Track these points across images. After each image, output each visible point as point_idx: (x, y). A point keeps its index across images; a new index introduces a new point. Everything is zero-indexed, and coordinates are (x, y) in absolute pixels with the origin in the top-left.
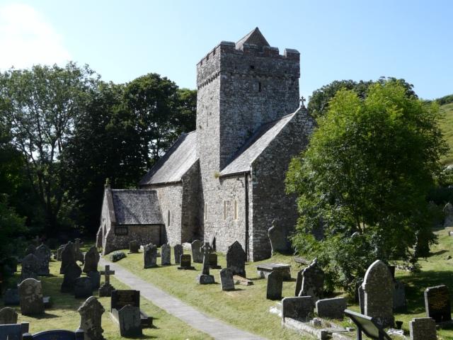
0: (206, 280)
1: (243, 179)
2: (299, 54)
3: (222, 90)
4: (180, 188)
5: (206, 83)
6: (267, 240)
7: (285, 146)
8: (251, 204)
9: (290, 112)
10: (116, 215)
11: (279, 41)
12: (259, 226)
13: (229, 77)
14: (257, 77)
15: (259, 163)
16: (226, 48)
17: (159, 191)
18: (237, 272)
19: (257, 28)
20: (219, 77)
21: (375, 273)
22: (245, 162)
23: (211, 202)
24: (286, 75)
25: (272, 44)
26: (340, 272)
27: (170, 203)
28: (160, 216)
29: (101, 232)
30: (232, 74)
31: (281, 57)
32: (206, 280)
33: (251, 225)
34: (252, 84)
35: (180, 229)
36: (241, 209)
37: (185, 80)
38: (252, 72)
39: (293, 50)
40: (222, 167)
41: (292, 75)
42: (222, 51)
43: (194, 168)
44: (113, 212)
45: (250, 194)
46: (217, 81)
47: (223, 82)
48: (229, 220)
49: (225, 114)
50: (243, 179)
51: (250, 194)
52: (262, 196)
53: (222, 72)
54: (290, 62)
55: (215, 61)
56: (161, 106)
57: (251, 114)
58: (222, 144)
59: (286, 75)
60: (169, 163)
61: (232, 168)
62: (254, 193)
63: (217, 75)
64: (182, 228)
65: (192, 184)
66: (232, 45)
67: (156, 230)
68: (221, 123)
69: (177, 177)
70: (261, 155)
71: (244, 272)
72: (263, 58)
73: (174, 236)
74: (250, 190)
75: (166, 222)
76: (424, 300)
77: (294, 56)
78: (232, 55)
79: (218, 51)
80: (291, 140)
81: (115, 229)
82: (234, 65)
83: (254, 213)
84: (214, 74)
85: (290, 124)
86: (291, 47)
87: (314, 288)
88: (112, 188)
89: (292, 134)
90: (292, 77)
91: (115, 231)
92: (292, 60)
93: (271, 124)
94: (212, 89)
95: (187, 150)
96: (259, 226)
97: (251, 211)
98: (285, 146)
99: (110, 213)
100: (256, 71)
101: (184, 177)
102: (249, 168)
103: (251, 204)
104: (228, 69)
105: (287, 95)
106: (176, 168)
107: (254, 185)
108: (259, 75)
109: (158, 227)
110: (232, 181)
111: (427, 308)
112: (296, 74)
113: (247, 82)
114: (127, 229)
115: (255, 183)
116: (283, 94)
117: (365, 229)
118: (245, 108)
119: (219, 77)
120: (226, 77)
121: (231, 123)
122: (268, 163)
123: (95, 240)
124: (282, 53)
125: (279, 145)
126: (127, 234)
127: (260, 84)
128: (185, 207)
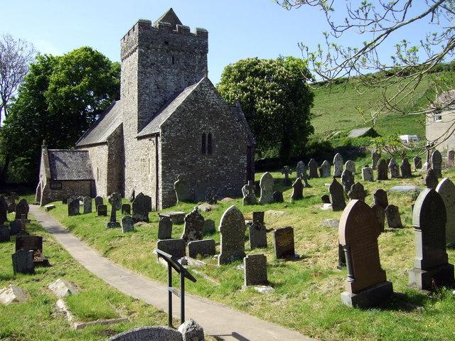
0: (113, 224)
1: (154, 139)
2: (207, 33)
3: (140, 62)
4: (106, 147)
5: (128, 56)
6: (174, 191)
7: (190, 111)
8: (160, 161)
9: (190, 84)
10: (51, 171)
11: (191, 21)
12: (167, 180)
13: (146, 51)
15: (167, 125)
16: (144, 25)
17: (90, 150)
18: (142, 219)
20: (137, 50)
22: (156, 126)
23: (131, 160)
24: (196, 51)
25: (185, 23)
26: (248, 228)
27: (99, 159)
28: (91, 172)
29: (40, 187)
30: (148, 49)
31: (192, 34)
32: (113, 224)
33: (160, 179)
34: (166, 57)
35: (106, 184)
36: (153, 165)
37: (112, 54)
38: (166, 47)
39: (203, 29)
40: (140, 129)
43: (119, 131)
44: (49, 169)
45: (160, 152)
46: (136, 54)
47: (141, 55)
48: (144, 174)
50: (154, 139)
51: (160, 152)
52: (170, 154)
53: (140, 46)
55: (134, 36)
56: (91, 79)
57: (166, 84)
58: (140, 109)
59: (196, 51)
63: (136, 49)
65: (117, 145)
66: (149, 23)
67: (87, 185)
68: (139, 91)
69: (103, 139)
70: (169, 119)
73: (102, 190)
74: (160, 149)
75: (96, 178)
76: (41, 157)
77: (203, 35)
79: (137, 27)
81: (51, 184)
83: (162, 168)
84: (133, 48)
85: (194, 92)
86: (201, 27)
87: (195, 232)
88: (48, 148)
89: (196, 100)
93: (177, 94)
94: (132, 62)
95: (116, 115)
96: (167, 180)
97: (160, 166)
98: (190, 111)
99: (46, 170)
100: (170, 47)
101: (109, 139)
103: (160, 161)
104: (145, 43)
105: (197, 68)
106: (105, 131)
107: (162, 145)
108: (172, 50)
109: (89, 182)
110: (147, 140)
111: (347, 264)
112: (204, 50)
116: (194, 67)
118: (160, 79)
119: (137, 50)
121: (148, 91)
122: (175, 125)
123: (35, 193)
124: (193, 31)
125: (184, 110)
126: (61, 188)
128: (110, 165)
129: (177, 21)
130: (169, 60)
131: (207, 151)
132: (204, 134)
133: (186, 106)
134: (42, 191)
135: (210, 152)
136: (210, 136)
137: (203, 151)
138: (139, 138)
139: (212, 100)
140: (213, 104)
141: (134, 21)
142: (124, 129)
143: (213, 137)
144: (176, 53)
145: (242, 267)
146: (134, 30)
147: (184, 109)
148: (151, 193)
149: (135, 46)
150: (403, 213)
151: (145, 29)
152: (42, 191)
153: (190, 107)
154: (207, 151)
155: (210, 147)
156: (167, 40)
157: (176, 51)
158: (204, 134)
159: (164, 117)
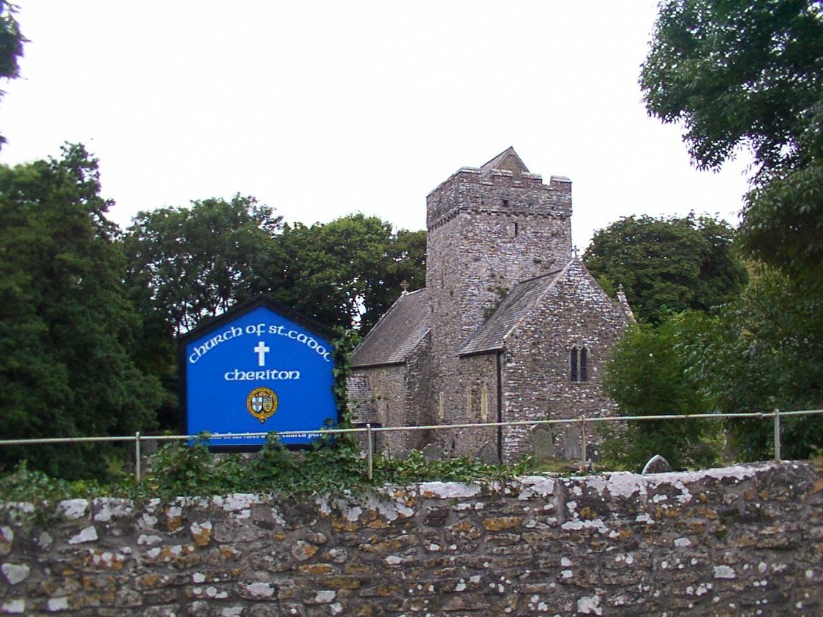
5: (440, 224)
11: (541, 166)
24: (553, 213)
43: (820, 495)
59: (553, 213)
77: (563, 186)
80: (560, 305)
82: (480, 200)
89: (561, 297)
90: (561, 216)
129: (520, 166)
130: (510, 229)
131: (579, 377)
132: (575, 350)
135: (584, 378)
136: (584, 351)
140: (588, 302)
141: (571, 180)
143: (589, 355)
144: (522, 217)
147: (543, 311)
154: (579, 377)
155: (584, 369)
156: (505, 198)
158: (575, 350)
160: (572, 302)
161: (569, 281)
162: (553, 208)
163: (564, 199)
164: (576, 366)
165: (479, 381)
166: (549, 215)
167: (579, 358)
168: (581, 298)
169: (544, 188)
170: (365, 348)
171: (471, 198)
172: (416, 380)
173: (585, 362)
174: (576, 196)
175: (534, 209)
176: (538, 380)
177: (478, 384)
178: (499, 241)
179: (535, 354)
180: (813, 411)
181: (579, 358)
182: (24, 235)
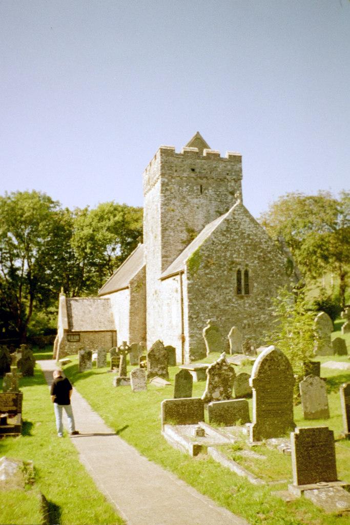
4: (127, 292)
13: (169, 181)
14: (199, 180)
18: (160, 373)
19: (198, 133)
21: (267, 364)
24: (228, 177)
28: (112, 322)
38: (193, 175)
41: (234, 177)
42: (161, 155)
43: (142, 275)
49: (165, 217)
50: (178, 277)
54: (233, 164)
59: (228, 177)
60: (327, 320)
61: (171, 270)
62: (189, 292)
64: (130, 333)
65: (139, 286)
67: (108, 336)
71: (167, 373)
72: (203, 161)
77: (236, 159)
78: (171, 159)
80: (228, 237)
82: (174, 169)
84: (155, 178)
89: (228, 230)
90: (234, 179)
91: (67, 338)
92: (234, 162)
102: (185, 268)
104: (168, 172)
106: (124, 275)
109: (110, 333)
113: (187, 185)
114: (79, 335)
115: (190, 282)
117: (69, 271)
118: (186, 211)
120: (166, 180)
126: (79, 341)
127: (201, 186)
132: (239, 272)
133: (215, 238)
134: (59, 344)
135: (247, 292)
136: (246, 273)
137: (239, 290)
138: (163, 279)
139: (246, 227)
142: (147, 269)
143: (251, 274)
145: (287, 444)
146: (156, 159)
148: (177, 345)
149: (157, 176)
150: (304, 240)
151: (168, 155)
152: (59, 344)
153: (221, 238)
155: (247, 285)
156: (193, 167)
157: (205, 179)
159: (189, 252)
160: (237, 234)
161: (234, 218)
162: (228, 174)
163: (236, 168)
164: (240, 283)
165: (171, 297)
166: (225, 178)
167: (243, 277)
168: (244, 231)
169: (222, 160)
170: (111, 279)
171: (168, 167)
172: (136, 299)
173: (248, 279)
174: (245, 165)
175: (213, 175)
176: (84, 260)
177: (170, 299)
178: (188, 197)
179: (208, 274)
180: (187, 399)
181: (243, 277)
182: (345, 324)
